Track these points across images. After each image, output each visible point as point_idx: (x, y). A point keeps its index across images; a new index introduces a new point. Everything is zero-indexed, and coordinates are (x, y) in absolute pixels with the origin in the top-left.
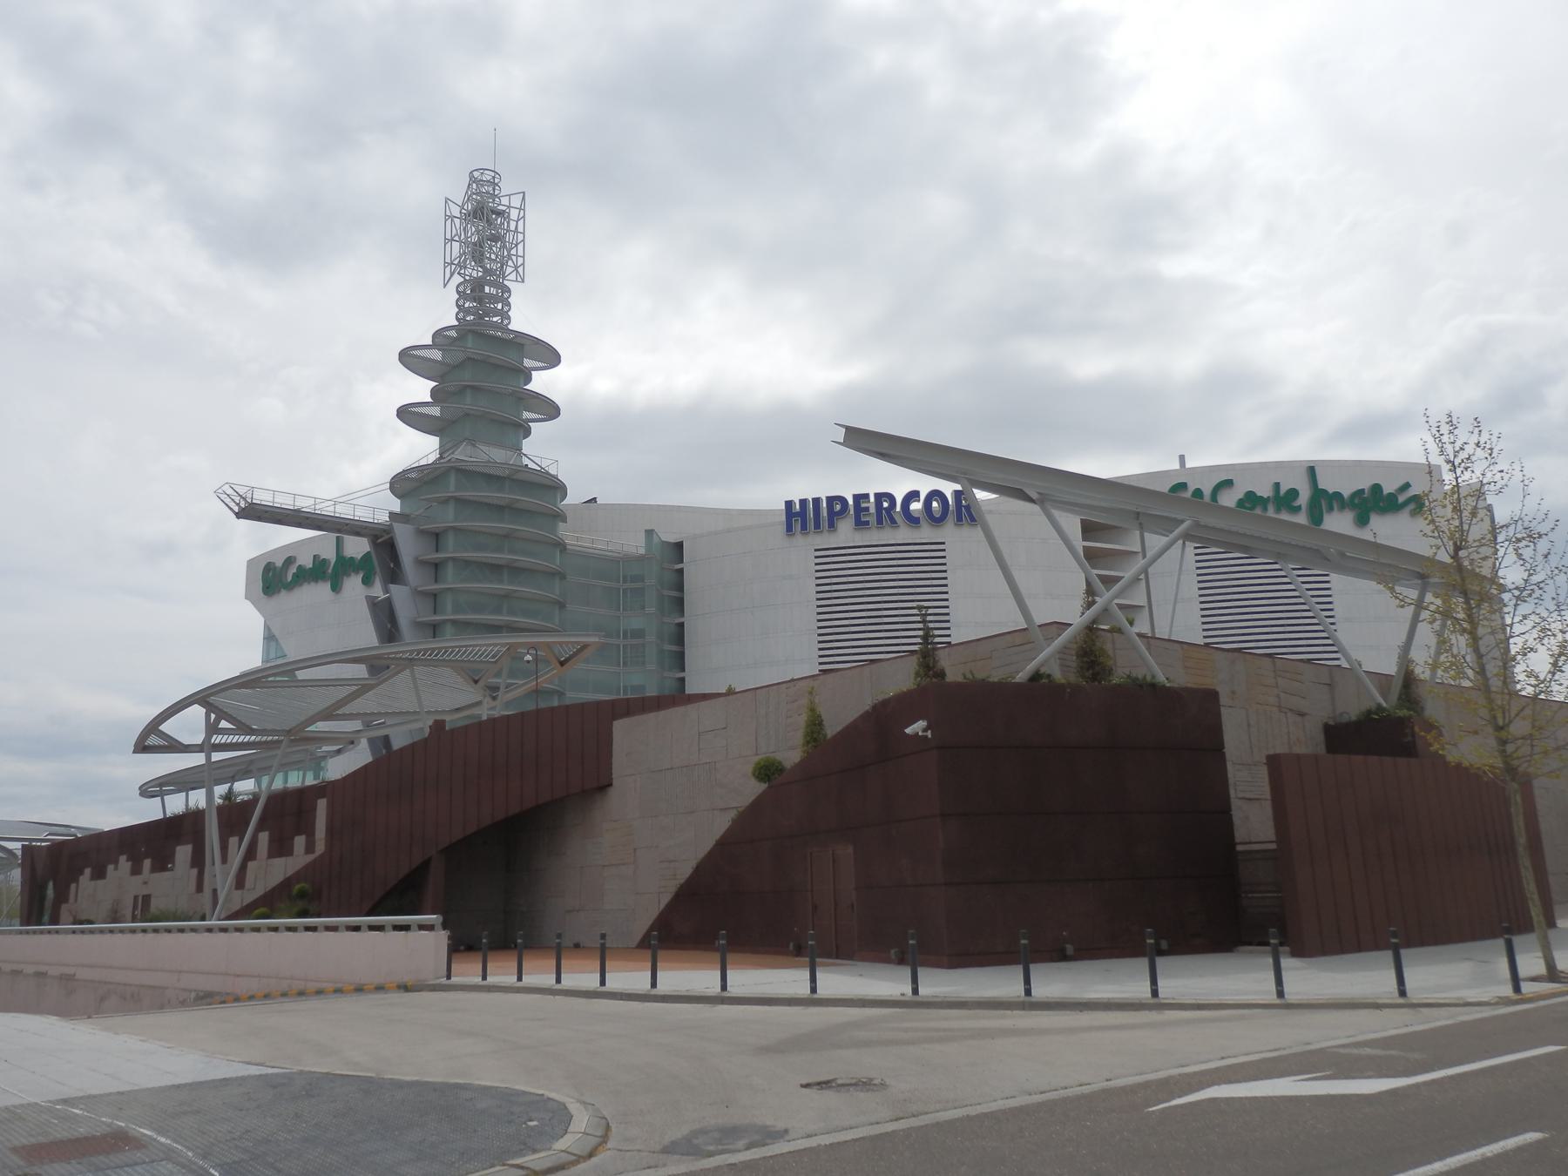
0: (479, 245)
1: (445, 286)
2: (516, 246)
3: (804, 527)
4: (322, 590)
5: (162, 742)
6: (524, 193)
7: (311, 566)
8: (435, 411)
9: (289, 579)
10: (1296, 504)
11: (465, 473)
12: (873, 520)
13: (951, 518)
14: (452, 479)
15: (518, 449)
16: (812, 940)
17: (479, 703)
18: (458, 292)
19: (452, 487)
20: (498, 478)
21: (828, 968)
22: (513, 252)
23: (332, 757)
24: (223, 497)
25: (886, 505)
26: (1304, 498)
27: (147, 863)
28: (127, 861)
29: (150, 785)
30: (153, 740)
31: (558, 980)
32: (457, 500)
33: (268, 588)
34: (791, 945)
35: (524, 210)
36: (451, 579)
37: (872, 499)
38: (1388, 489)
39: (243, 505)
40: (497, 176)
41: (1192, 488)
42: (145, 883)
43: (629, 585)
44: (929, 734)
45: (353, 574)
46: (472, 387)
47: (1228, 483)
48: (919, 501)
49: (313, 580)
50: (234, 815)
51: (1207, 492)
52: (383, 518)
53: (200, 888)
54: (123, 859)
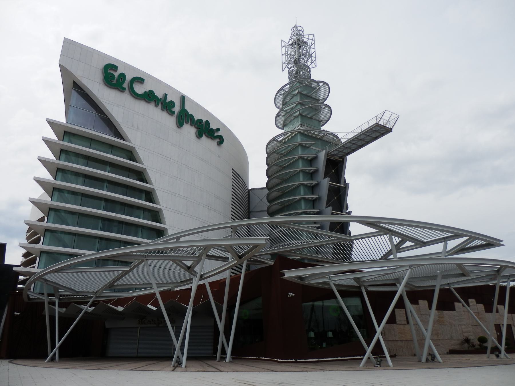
4: (170, 121)
6: (314, 34)
10: (174, 110)
14: (303, 203)
21: (297, 364)
26: (177, 109)
35: (314, 40)
38: (213, 126)
41: (120, 70)
47: (140, 80)
51: (129, 78)
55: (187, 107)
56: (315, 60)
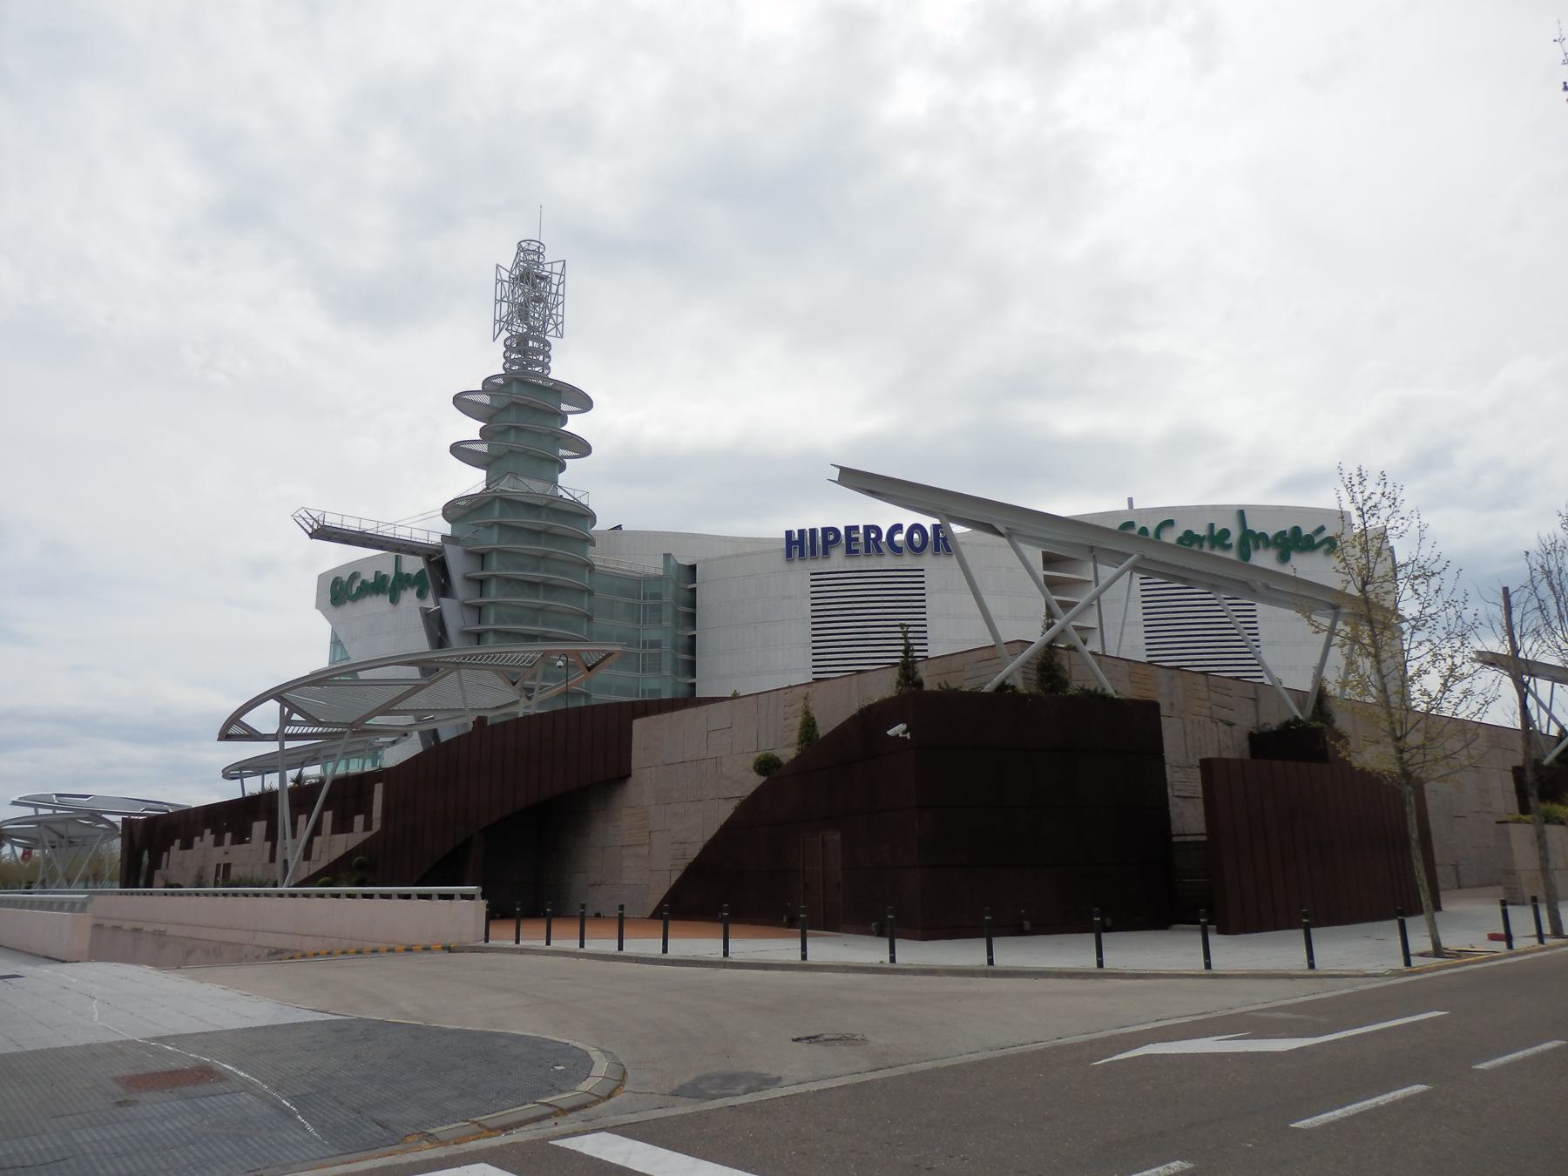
0: (525, 305)
1: (494, 340)
2: (557, 306)
3: (802, 554)
4: (380, 603)
5: (243, 732)
7: (373, 581)
8: (484, 448)
9: (354, 591)
11: (508, 502)
12: (862, 548)
13: (930, 547)
14: (497, 506)
15: (555, 482)
16: (1097, 917)
17: (517, 702)
18: (505, 345)
19: (496, 514)
20: (537, 507)
22: (554, 311)
23: (387, 747)
24: (299, 519)
25: (873, 536)
26: (1234, 538)
27: (228, 836)
28: (212, 834)
29: (232, 768)
30: (235, 730)
31: (582, 945)
32: (502, 526)
33: (335, 599)
34: (785, 918)
36: (493, 592)
37: (861, 531)
38: (1307, 530)
39: (315, 527)
40: (542, 246)
42: (227, 853)
43: (650, 602)
44: (908, 735)
45: (409, 588)
46: (517, 428)
47: (1169, 523)
48: (902, 533)
49: (367, 594)
50: (303, 796)
51: (1152, 530)
52: (436, 539)
53: (272, 859)
54: (207, 832)
55: (1252, 525)
56: (562, 322)
